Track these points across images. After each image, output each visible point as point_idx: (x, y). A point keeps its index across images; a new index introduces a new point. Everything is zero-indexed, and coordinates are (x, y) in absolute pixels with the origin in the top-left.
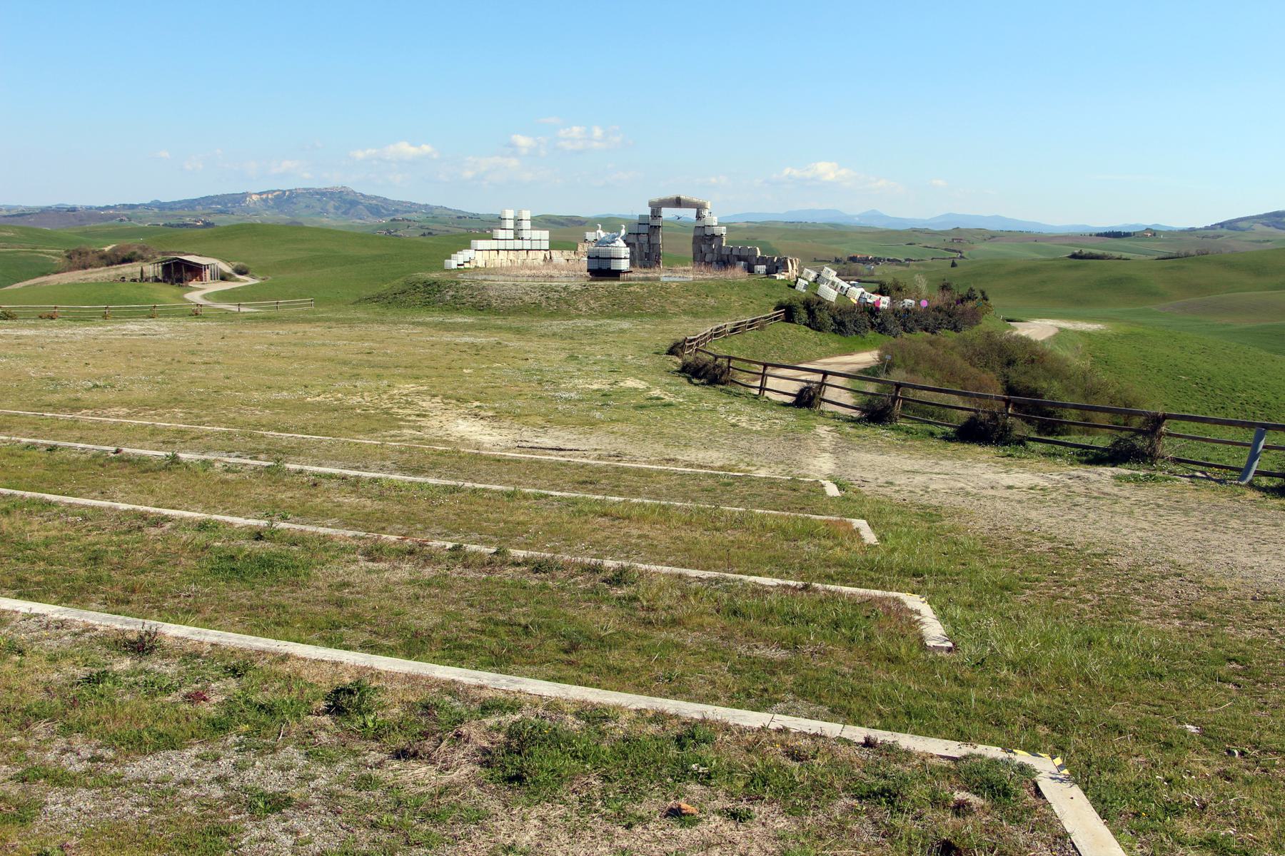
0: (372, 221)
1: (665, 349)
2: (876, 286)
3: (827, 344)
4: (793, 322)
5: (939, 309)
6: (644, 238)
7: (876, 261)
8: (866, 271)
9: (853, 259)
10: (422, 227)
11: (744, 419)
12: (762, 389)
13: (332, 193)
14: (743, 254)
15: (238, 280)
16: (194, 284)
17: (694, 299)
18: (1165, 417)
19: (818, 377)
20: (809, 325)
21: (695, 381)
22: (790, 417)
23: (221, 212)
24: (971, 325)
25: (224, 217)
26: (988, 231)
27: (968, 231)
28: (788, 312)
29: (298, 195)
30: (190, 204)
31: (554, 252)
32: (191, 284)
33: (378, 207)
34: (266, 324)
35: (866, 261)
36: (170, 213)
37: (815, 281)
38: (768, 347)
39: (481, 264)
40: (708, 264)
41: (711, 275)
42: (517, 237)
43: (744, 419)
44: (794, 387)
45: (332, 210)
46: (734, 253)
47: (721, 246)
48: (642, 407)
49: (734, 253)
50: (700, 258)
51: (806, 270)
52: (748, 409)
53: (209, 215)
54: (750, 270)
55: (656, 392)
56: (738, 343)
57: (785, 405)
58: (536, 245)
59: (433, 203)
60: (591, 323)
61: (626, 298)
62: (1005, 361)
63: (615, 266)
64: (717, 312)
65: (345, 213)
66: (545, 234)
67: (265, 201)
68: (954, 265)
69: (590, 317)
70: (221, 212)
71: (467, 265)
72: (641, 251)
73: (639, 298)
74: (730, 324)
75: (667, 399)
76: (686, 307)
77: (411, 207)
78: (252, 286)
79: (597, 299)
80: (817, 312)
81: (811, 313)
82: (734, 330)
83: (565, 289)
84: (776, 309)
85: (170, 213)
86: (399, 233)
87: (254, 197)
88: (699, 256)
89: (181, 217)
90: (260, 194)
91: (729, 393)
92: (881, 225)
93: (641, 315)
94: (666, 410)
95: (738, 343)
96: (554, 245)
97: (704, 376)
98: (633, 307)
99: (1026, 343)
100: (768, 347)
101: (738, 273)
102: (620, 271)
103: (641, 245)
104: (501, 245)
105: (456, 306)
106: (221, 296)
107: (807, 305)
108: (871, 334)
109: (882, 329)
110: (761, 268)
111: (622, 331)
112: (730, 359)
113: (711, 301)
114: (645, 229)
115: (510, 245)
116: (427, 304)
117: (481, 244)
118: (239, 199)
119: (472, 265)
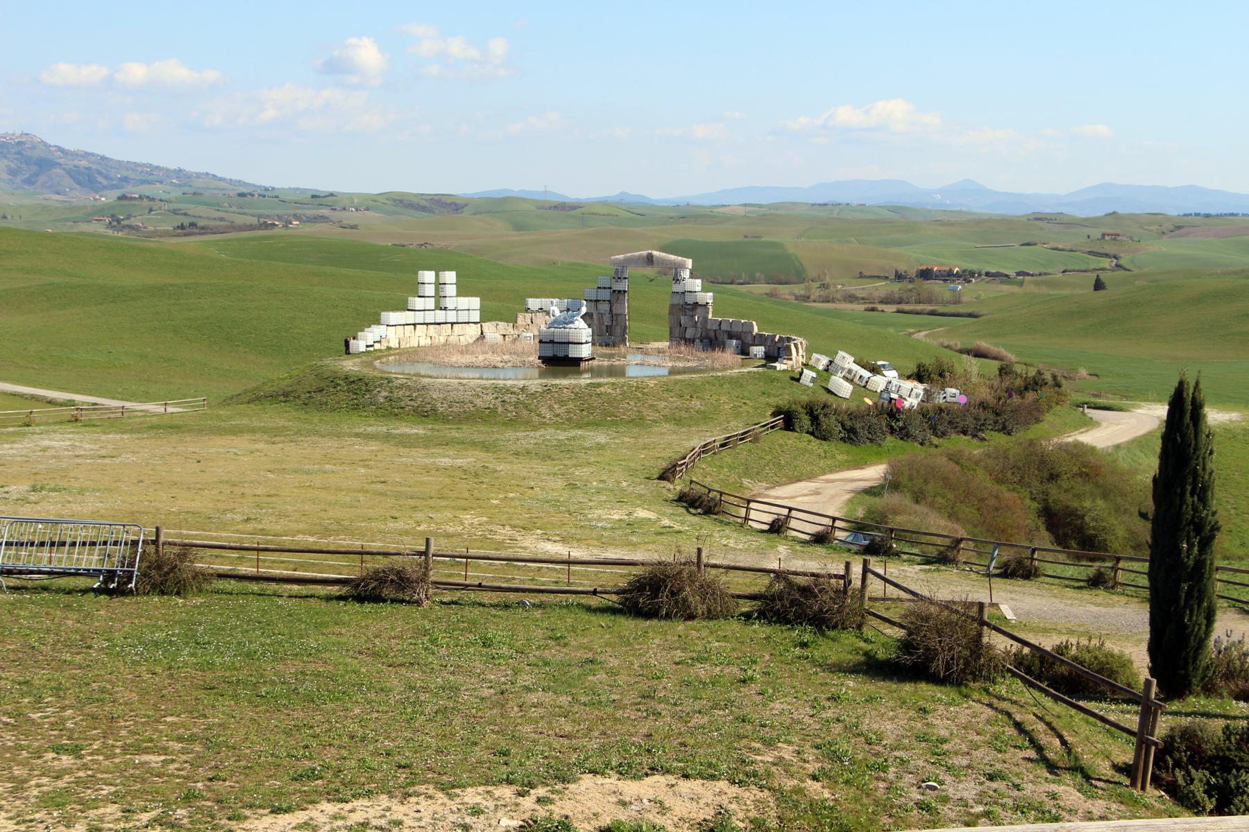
0: (80, 197)
2: (913, 368)
3: (833, 457)
4: (793, 430)
5: (983, 405)
6: (604, 307)
7: (966, 276)
8: (947, 296)
9: (926, 274)
10: (175, 212)
11: (732, 541)
12: (746, 519)
14: (735, 329)
17: (678, 402)
18: (962, 540)
19: (785, 512)
20: (812, 434)
21: (692, 510)
22: (762, 540)
24: (1027, 424)
26: (1167, 218)
27: (1133, 218)
28: (788, 420)
31: (487, 326)
33: (91, 172)
35: (948, 276)
37: (827, 370)
38: (763, 462)
39: (394, 344)
40: (690, 342)
41: (694, 358)
42: (439, 307)
43: (732, 541)
44: (769, 518)
47: (706, 319)
48: (661, 534)
50: (680, 336)
51: (815, 356)
52: (735, 535)
54: (744, 351)
55: (666, 522)
56: (728, 460)
57: (763, 531)
58: (463, 317)
59: (192, 167)
60: (562, 436)
61: (596, 402)
62: (1046, 475)
63: (574, 352)
64: (704, 418)
65: (29, 181)
68: (1099, 285)
69: (557, 426)
71: (377, 346)
73: (611, 401)
74: (720, 438)
75: (677, 527)
76: (667, 412)
77: (151, 174)
79: (562, 403)
80: (822, 418)
81: (815, 419)
82: (722, 445)
83: (523, 389)
84: (774, 414)
86: (133, 222)
88: (677, 331)
91: (721, 522)
92: (979, 207)
93: (614, 423)
94: (678, 536)
95: (728, 460)
96: (487, 315)
97: (699, 506)
98: (605, 414)
99: (1080, 453)
100: (763, 462)
101: (728, 357)
102: (581, 359)
103: (601, 315)
104: (419, 317)
105: (393, 409)
107: (811, 411)
108: (890, 441)
109: (904, 434)
110: (759, 350)
111: (600, 447)
112: (721, 494)
113: (696, 404)
114: (606, 295)
115: (430, 317)
116: (355, 408)
117: (394, 317)
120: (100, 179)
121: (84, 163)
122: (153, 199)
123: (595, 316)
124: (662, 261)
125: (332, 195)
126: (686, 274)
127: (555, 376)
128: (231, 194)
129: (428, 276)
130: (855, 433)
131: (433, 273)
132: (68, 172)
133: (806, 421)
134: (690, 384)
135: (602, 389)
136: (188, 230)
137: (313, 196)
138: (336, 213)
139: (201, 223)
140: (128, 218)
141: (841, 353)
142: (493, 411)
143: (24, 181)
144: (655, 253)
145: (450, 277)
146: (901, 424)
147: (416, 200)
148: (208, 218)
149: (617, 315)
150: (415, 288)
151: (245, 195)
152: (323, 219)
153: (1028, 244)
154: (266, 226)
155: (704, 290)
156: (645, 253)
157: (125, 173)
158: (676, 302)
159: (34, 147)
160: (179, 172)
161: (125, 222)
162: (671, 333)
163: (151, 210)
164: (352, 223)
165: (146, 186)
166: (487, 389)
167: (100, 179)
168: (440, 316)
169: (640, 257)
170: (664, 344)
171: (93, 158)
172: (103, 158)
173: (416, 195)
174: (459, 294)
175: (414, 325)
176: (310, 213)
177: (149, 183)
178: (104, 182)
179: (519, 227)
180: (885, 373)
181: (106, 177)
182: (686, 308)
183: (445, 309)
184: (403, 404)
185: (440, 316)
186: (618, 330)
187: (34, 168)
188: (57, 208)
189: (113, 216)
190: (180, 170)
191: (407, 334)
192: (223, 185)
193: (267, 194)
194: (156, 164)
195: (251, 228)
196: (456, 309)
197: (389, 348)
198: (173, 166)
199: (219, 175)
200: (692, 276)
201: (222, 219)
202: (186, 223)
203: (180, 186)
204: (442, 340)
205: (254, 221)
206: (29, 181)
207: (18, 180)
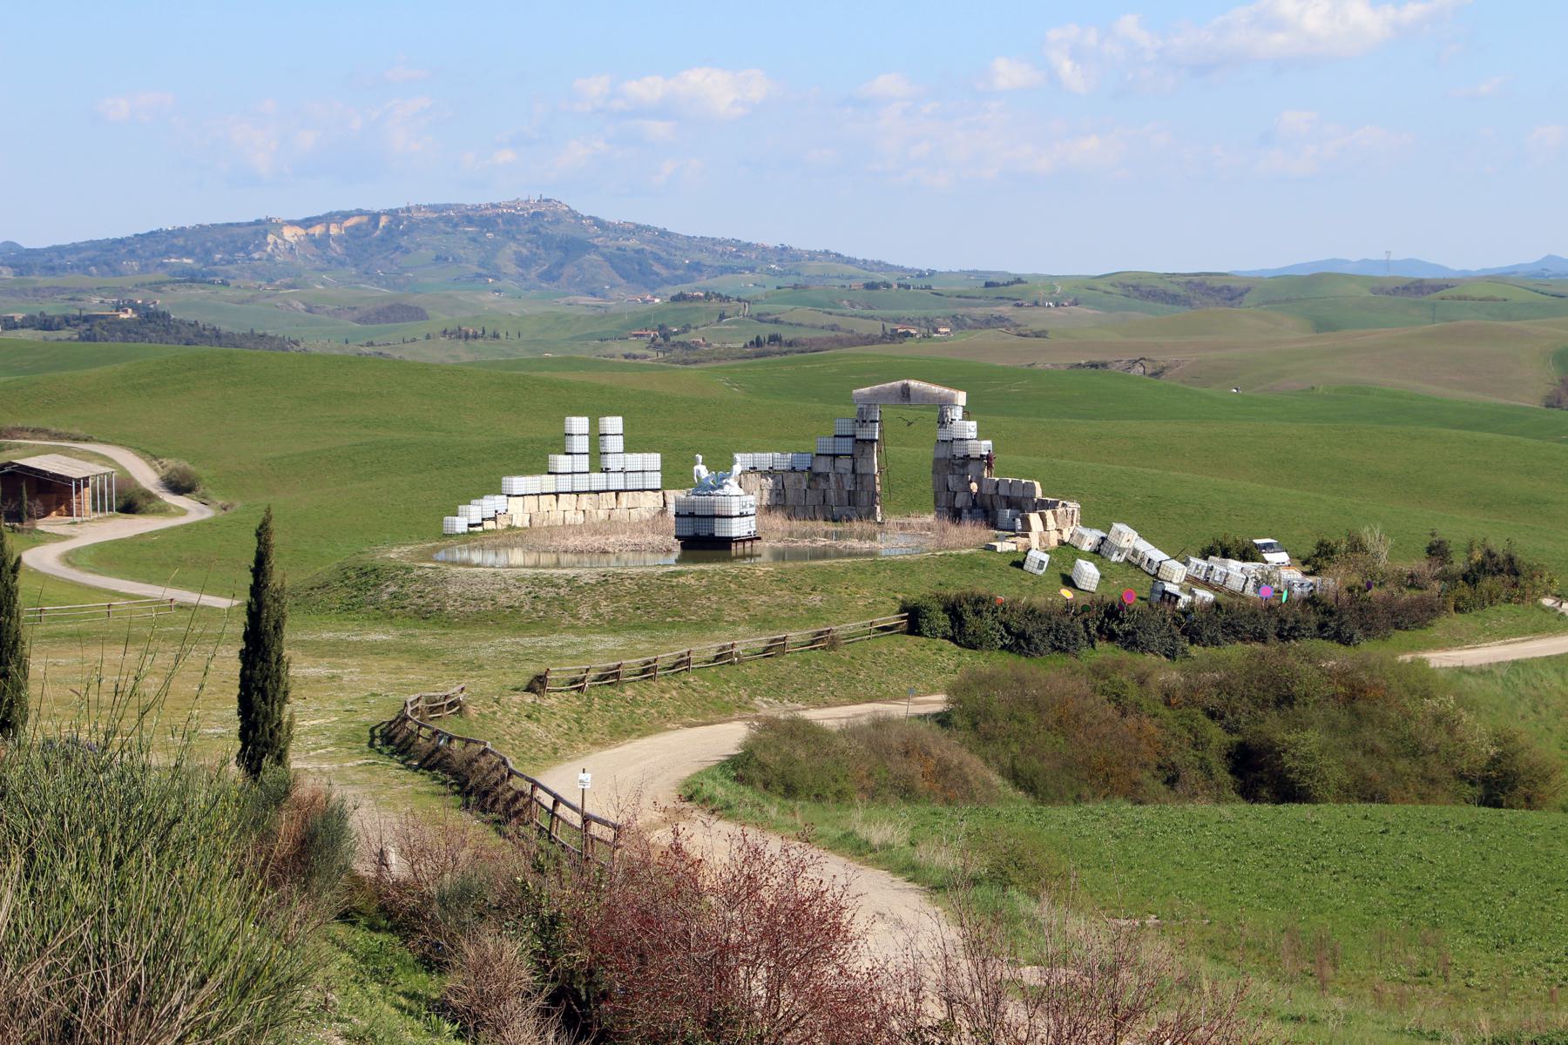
0: (626, 299)
2: (1309, 549)
4: (920, 634)
6: (844, 464)
10: (760, 318)
13: (512, 220)
15: (164, 510)
16: (51, 524)
20: (953, 639)
23: (192, 278)
25: (198, 292)
29: (413, 227)
30: (106, 254)
32: (42, 525)
33: (642, 256)
36: (44, 281)
39: (520, 521)
45: (512, 268)
46: (1003, 491)
53: (157, 286)
58: (635, 481)
59: (805, 240)
63: (721, 529)
65: (548, 276)
66: (653, 460)
67: (321, 243)
70: (192, 278)
71: (489, 525)
72: (840, 487)
77: (737, 256)
78: (198, 525)
79: (615, 598)
85: (44, 281)
86: (693, 337)
89: (75, 295)
90: (307, 223)
104: (564, 483)
106: (108, 557)
113: (816, 599)
114: (846, 446)
115: (581, 483)
116: (349, 608)
117: (518, 483)
118: (246, 238)
119: (503, 523)
120: (657, 268)
121: (633, 243)
122: (728, 298)
124: (925, 397)
125: (1019, 281)
126: (957, 414)
127: (696, 561)
128: (855, 284)
129: (579, 424)
130: (1028, 640)
131: (586, 419)
133: (943, 621)
135: (682, 580)
136: (766, 347)
137: (988, 285)
139: (787, 335)
140: (685, 330)
141: (1117, 526)
144: (913, 384)
145: (613, 424)
146: (1127, 626)
147: (1161, 285)
148: (813, 327)
150: (560, 444)
152: (1001, 320)
154: (895, 337)
155: (982, 435)
156: (898, 384)
157: (698, 256)
161: (681, 338)
162: (936, 501)
163: (722, 317)
164: (1037, 327)
166: (523, 580)
168: (598, 481)
169: (892, 391)
170: (930, 518)
171: (647, 235)
172: (664, 233)
173: (1162, 276)
174: (629, 447)
175: (557, 494)
176: (979, 312)
178: (664, 272)
179: (1323, 326)
180: (1267, 556)
181: (667, 265)
182: (954, 463)
183: (607, 471)
185: (598, 481)
186: (864, 497)
187: (559, 254)
188: (578, 318)
190: (784, 249)
191: (544, 508)
192: (852, 269)
193: (921, 284)
195: (869, 340)
197: (510, 527)
198: (772, 242)
200: (967, 415)
201: (834, 328)
202: (764, 336)
203: (781, 274)
205: (875, 328)
207: (533, 273)
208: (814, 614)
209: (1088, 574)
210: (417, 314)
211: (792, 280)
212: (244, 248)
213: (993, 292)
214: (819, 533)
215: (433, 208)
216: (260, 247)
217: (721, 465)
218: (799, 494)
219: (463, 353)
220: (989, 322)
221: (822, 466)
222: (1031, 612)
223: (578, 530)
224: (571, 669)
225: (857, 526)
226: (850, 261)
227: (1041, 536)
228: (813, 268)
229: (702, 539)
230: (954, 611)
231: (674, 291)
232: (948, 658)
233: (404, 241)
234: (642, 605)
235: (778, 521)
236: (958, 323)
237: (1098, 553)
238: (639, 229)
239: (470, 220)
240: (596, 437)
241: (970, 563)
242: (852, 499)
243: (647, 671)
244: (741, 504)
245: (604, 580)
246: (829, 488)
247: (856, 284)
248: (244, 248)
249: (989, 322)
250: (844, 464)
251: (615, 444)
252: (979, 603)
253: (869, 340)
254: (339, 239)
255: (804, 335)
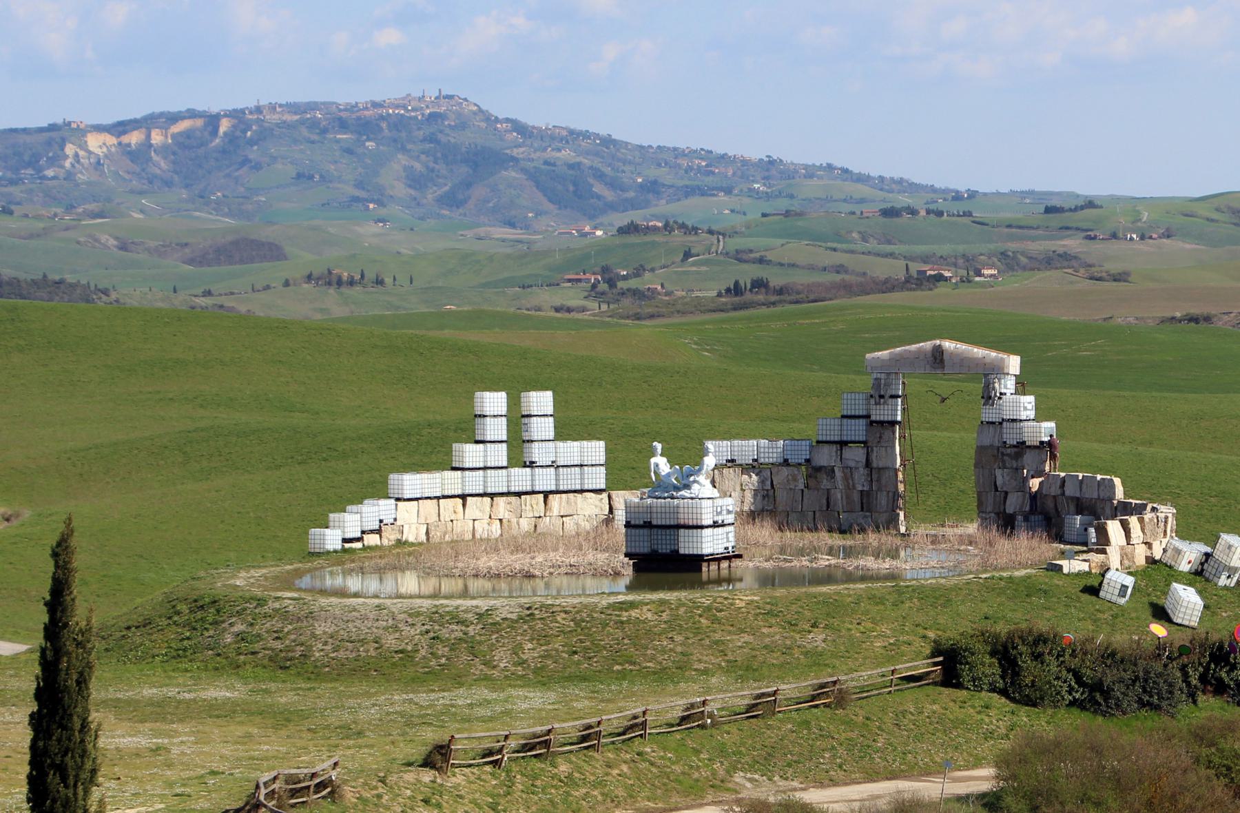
0: (557, 231)
1: (420, 760)
4: (959, 686)
6: (855, 455)
10: (739, 256)
13: (399, 124)
20: (1003, 693)
29: (265, 134)
31: (614, 494)
33: (579, 172)
34: (360, 687)
39: (414, 534)
45: (401, 190)
46: (1070, 491)
49: (1070, 491)
58: (570, 479)
59: (793, 153)
63: (689, 545)
65: (452, 200)
66: (595, 450)
67: (139, 155)
71: (371, 540)
77: (708, 172)
79: (542, 638)
86: (649, 281)
87: (95, 142)
88: (990, 498)
90: (120, 128)
103: (849, 471)
104: (474, 482)
113: (817, 639)
114: (857, 430)
115: (497, 481)
116: (179, 654)
117: (411, 483)
119: (390, 537)
120: (598, 188)
121: (566, 154)
122: (695, 230)
123: (838, 474)
124: (964, 362)
125: (1090, 204)
127: (654, 587)
128: (867, 209)
129: (494, 402)
130: (1107, 694)
132: (534, 176)
133: (989, 668)
134: (825, 601)
135: (634, 613)
137: (1049, 210)
138: (1097, 246)
140: (638, 272)
142: (407, 656)
143: (441, 201)
144: (948, 345)
145: (541, 401)
148: (812, 268)
149: (879, 469)
151: (898, 210)
152: (1065, 259)
153: (1194, 319)
156: (927, 345)
157: (653, 173)
158: (987, 442)
159: (462, 125)
160: (769, 166)
161: (633, 283)
162: (980, 504)
163: (687, 255)
164: (1114, 267)
165: (696, 200)
166: (418, 614)
167: (598, 188)
168: (520, 478)
170: (972, 528)
172: (608, 141)
175: (463, 497)
177: (702, 192)
178: (609, 195)
181: (613, 184)
182: (1004, 453)
183: (532, 465)
184: (257, 647)
186: (883, 500)
187: (464, 170)
189: (605, 270)
191: (446, 515)
192: (863, 190)
194: (719, 150)
195: (888, 286)
196: (554, 465)
197: (400, 543)
198: (755, 152)
199: (855, 169)
200: (1022, 386)
201: (839, 269)
202: (745, 281)
203: (768, 196)
204: (526, 524)
205: (895, 269)
206: (452, 200)
207: (431, 195)
208: (816, 659)
209: (1188, 602)
210: (272, 252)
211: (783, 204)
212: (33, 163)
213: (1055, 220)
214: (820, 550)
215: (293, 108)
216: (56, 160)
217: (688, 457)
218: (787, 497)
219: (334, 305)
220: (1050, 261)
221: (825, 457)
222: (1110, 656)
223: (493, 546)
224: (484, 735)
225: (873, 538)
226: (862, 179)
227: (1125, 550)
228: (810, 189)
229: (662, 558)
230: (1004, 653)
231: (622, 219)
232: (998, 717)
233: (253, 153)
234: (578, 648)
235: (765, 533)
236: (1008, 262)
237: (1200, 575)
238: (574, 136)
239: (343, 125)
240: (517, 419)
241: (1026, 590)
242: (866, 502)
243: (588, 738)
244: (715, 510)
245: (529, 615)
246: (837, 487)
247: (871, 209)
248: (33, 163)
249: (1050, 261)
250: (855, 455)
251: (542, 428)
252: (1039, 642)
253: (888, 286)
254: (164, 150)
255: (800, 279)
